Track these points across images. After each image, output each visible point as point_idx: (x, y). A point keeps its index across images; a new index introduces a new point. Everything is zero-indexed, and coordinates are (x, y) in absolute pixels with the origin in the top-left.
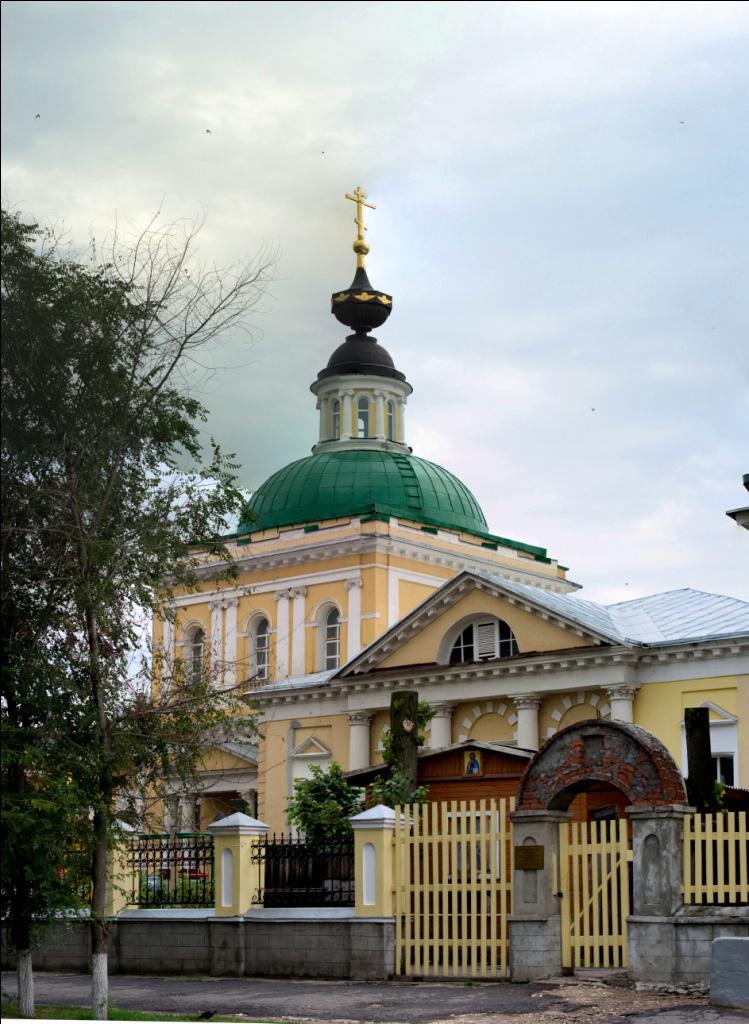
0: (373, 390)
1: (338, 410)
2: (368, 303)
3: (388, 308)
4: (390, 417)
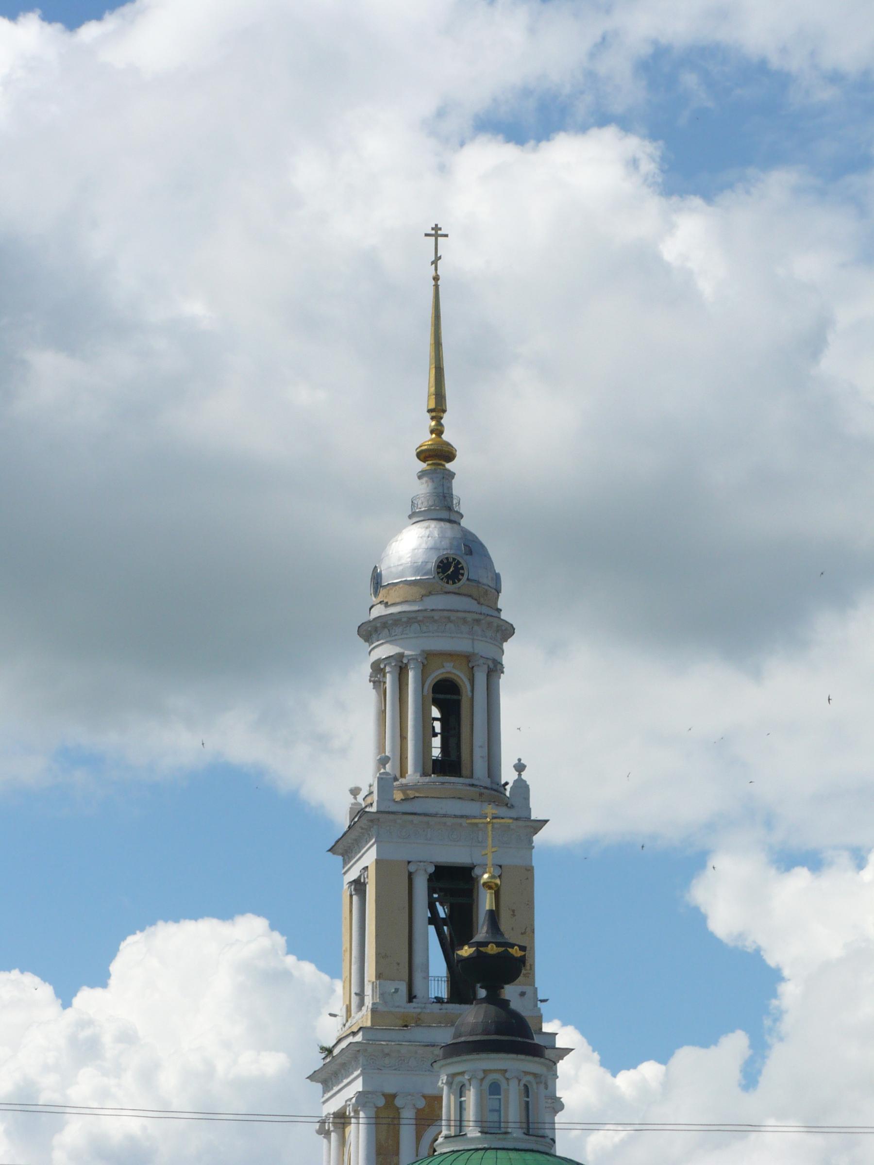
0: (506, 1071)
4: (527, 1103)
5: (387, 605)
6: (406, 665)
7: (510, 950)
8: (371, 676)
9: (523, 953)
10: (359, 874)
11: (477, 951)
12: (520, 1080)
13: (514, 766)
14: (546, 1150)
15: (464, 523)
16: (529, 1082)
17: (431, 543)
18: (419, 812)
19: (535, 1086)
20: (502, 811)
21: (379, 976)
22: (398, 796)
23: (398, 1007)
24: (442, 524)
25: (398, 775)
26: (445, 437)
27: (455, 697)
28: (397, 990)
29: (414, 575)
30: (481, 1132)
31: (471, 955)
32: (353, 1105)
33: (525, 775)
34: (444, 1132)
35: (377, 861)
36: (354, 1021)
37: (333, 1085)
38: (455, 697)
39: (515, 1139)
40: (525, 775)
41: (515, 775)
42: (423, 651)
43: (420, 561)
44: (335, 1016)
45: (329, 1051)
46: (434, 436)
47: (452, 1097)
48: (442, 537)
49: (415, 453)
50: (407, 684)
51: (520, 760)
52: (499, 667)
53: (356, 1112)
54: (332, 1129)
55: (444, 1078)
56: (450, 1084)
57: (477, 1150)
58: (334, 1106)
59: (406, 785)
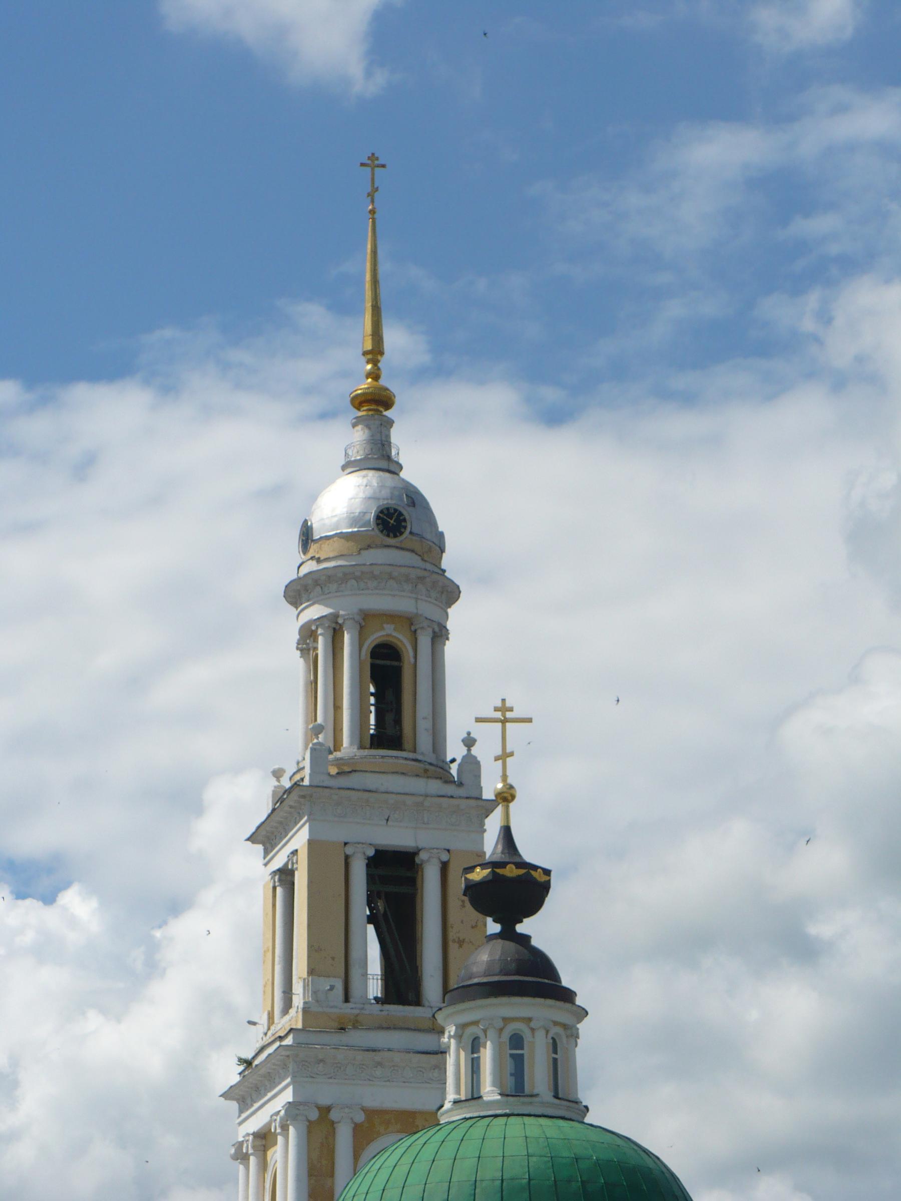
0: (530, 1019)
1: (478, 1051)
2: (518, 880)
3: (545, 888)
4: (555, 1061)
5: (319, 561)
6: (341, 626)
7: (533, 873)
8: (298, 644)
9: (547, 878)
10: (286, 860)
11: (493, 873)
12: (547, 1032)
13: (463, 741)
14: (581, 1120)
15: (403, 474)
16: (557, 1034)
17: (369, 492)
18: (356, 787)
19: (564, 1040)
20: (450, 789)
21: (311, 971)
22: (333, 771)
23: (332, 1007)
24: (381, 473)
25: (332, 749)
26: (383, 382)
27: (395, 663)
28: (332, 988)
29: (351, 527)
30: (500, 1094)
31: (484, 877)
32: (281, 1118)
33: (475, 751)
34: (451, 1096)
35: (311, 842)
36: (279, 1026)
37: (254, 1101)
38: (395, 663)
39: (543, 1103)
40: (475, 751)
41: (464, 751)
42: (361, 610)
43: (358, 511)
44: (254, 1024)
45: (248, 1063)
46: (370, 380)
47: (462, 1054)
48: (382, 486)
49: (349, 399)
50: (342, 649)
51: (469, 734)
52: (444, 632)
53: (285, 1128)
54: (251, 1151)
55: (451, 1030)
56: (459, 1037)
57: (496, 1116)
58: (255, 1124)
59: (341, 759)
